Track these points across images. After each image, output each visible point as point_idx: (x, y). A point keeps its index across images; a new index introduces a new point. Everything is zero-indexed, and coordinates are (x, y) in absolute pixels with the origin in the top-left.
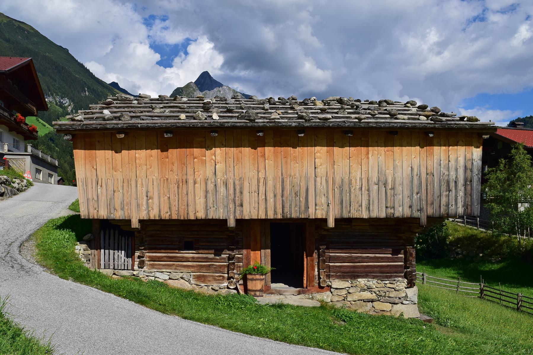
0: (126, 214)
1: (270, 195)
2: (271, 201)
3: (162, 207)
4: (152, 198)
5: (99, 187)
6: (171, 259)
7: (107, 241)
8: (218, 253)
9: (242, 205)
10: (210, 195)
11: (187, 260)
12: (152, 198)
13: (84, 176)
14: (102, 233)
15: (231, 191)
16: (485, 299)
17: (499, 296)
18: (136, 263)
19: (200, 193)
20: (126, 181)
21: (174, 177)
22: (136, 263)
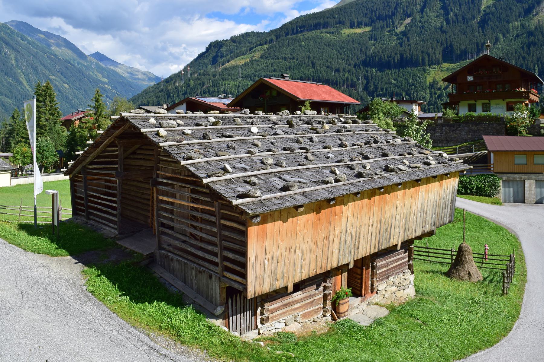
0: (285, 282)
1: (374, 235)
2: (374, 239)
3: (311, 267)
4: (305, 260)
5: (266, 262)
6: (286, 305)
7: (234, 308)
8: (318, 286)
9: (358, 248)
10: (342, 245)
11: (297, 302)
12: (305, 260)
13: (255, 254)
14: (230, 301)
15: (354, 239)
16: (294, 104)
17: (427, 254)
18: (259, 321)
19: (336, 245)
20: (288, 250)
21: (321, 235)
22: (259, 321)
